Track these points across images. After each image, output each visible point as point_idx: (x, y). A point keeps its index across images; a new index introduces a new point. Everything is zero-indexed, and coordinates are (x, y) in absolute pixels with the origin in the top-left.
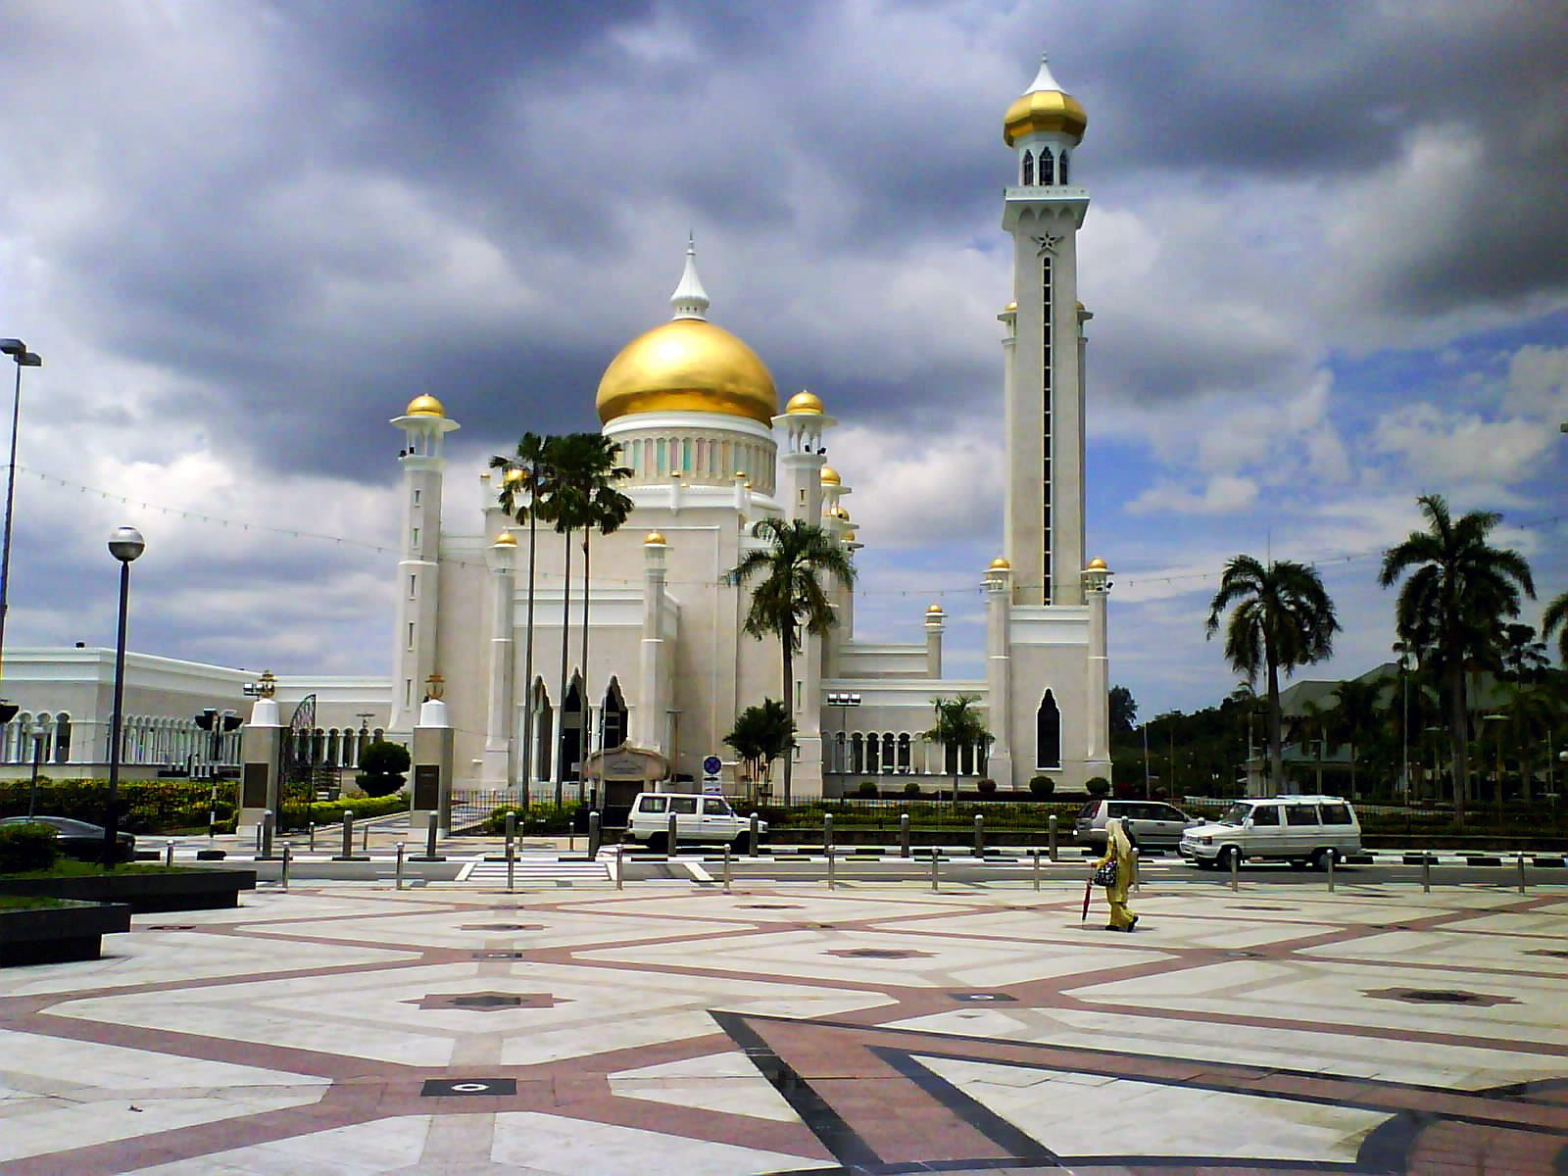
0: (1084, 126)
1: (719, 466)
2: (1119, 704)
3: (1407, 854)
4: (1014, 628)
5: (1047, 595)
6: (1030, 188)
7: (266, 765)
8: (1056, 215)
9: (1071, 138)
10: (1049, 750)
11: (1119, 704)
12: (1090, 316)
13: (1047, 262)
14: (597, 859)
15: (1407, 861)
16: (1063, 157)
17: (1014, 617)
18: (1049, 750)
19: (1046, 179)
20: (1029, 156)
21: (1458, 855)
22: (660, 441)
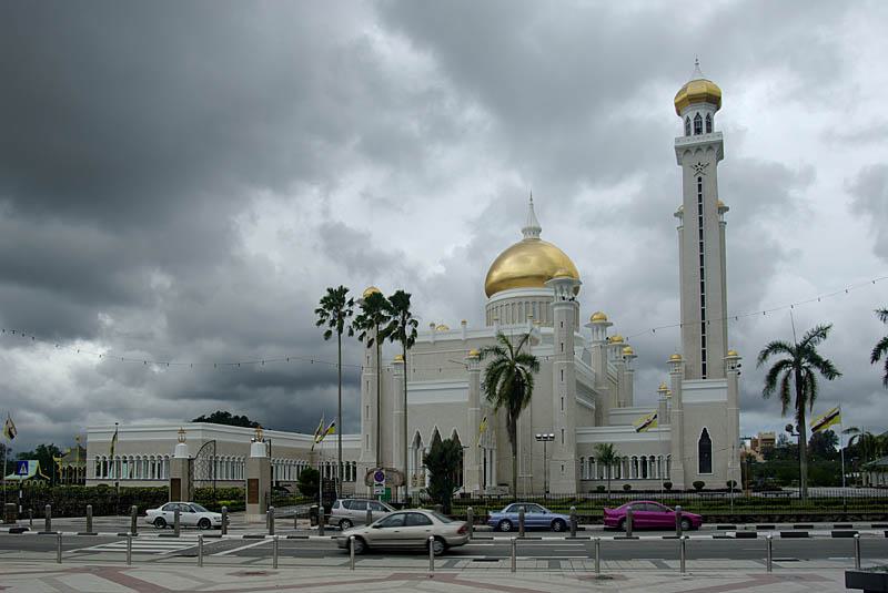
0: (720, 98)
1: (544, 316)
2: (437, 435)
3: (836, 527)
4: (684, 393)
5: (704, 373)
6: (700, 136)
7: (846, 573)
8: (705, 150)
9: (713, 107)
10: (705, 465)
11: (437, 435)
12: (727, 209)
13: (700, 179)
14: (400, 468)
15: (834, 535)
16: (708, 117)
17: (684, 387)
18: (705, 465)
19: (698, 131)
20: (688, 120)
21: (874, 527)
22: (534, 303)
